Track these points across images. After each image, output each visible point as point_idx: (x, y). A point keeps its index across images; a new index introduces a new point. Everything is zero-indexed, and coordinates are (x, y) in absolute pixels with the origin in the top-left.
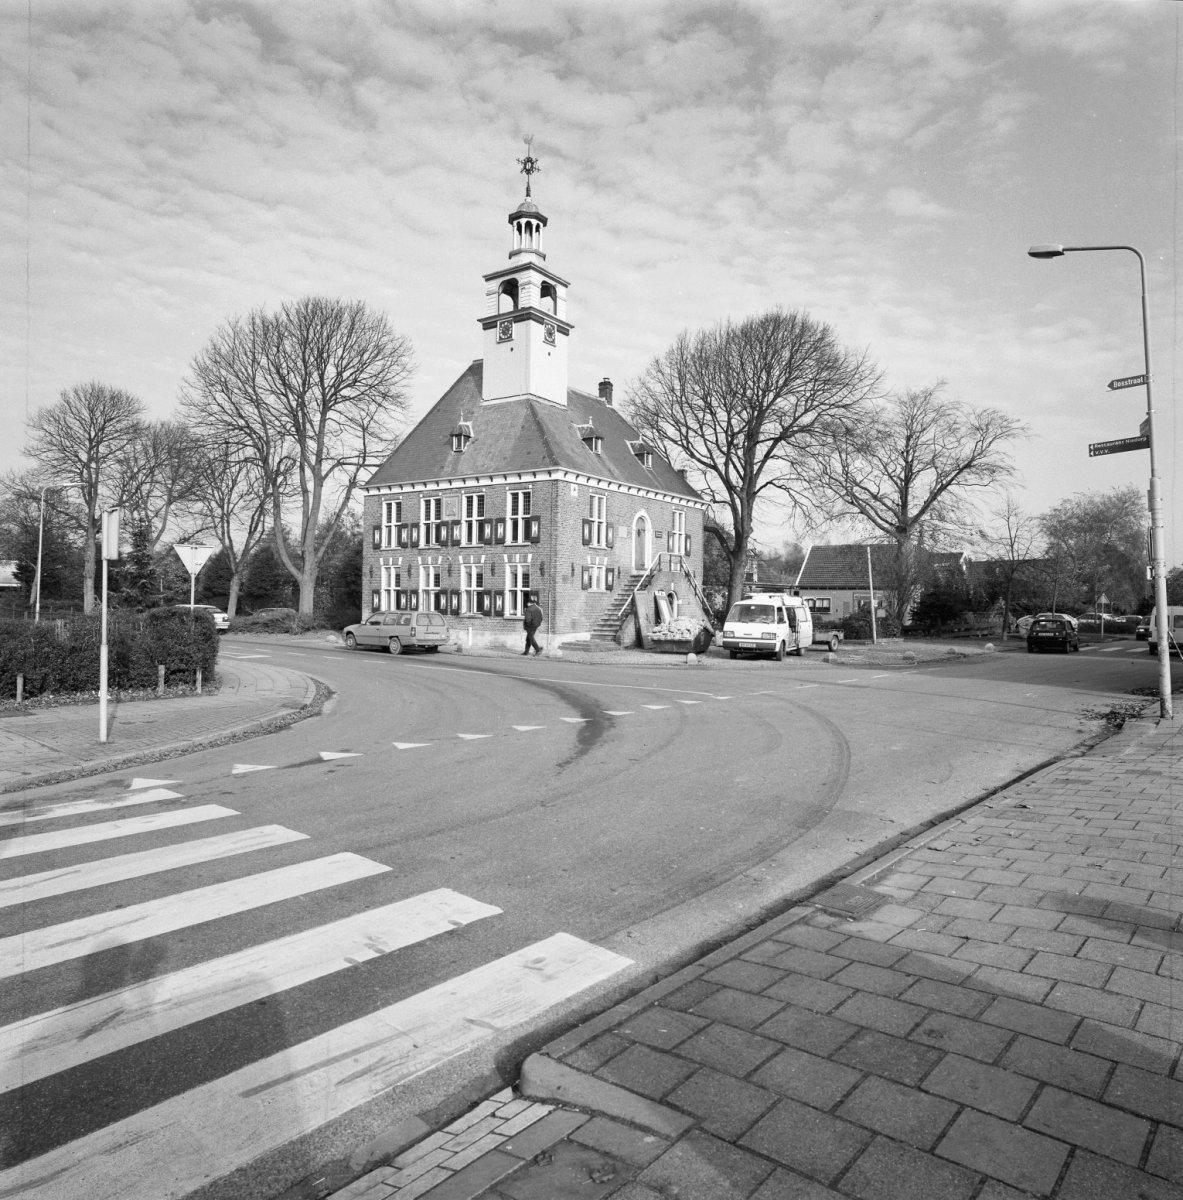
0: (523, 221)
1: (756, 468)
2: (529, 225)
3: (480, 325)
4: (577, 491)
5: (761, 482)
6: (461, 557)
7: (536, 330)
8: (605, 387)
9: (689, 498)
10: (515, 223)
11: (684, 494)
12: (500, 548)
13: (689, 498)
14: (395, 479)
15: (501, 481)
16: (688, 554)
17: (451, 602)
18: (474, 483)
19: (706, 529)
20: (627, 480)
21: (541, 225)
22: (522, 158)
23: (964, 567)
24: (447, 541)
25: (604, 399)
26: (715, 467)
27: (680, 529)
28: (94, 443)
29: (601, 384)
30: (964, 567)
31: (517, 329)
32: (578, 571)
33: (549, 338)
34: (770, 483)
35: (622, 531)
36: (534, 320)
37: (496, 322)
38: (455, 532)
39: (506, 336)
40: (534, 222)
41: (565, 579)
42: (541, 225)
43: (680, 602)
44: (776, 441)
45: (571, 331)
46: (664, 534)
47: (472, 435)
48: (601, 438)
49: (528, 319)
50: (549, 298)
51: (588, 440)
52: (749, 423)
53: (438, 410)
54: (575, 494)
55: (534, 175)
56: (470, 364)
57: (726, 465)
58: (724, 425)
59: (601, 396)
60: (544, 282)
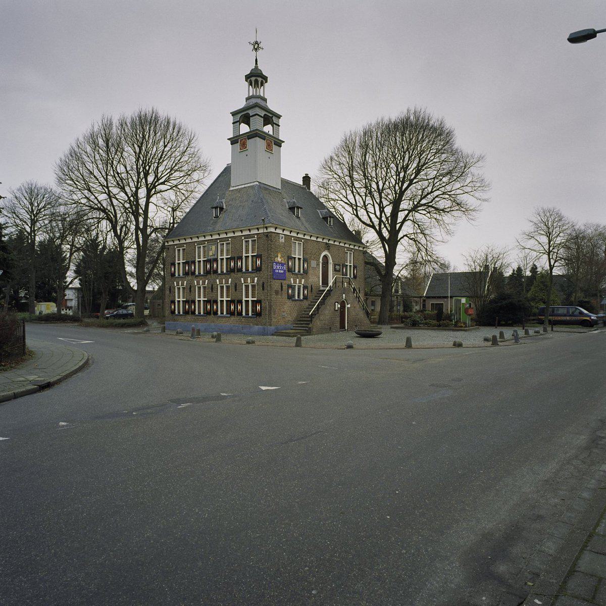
0: (253, 79)
1: (398, 226)
2: (256, 81)
3: (229, 142)
4: (283, 238)
5: (400, 235)
6: (218, 280)
7: (260, 143)
8: (307, 179)
9: (351, 243)
10: (248, 80)
11: (352, 241)
12: (240, 274)
13: (351, 243)
14: (176, 236)
15: (239, 234)
16: (355, 277)
17: (191, 307)
18: (224, 236)
19: (366, 263)
20: (339, 238)
21: (264, 81)
22: (252, 42)
23: (100, 247)
24: (188, 273)
25: (304, 186)
26: (373, 227)
27: (350, 263)
28: (34, 222)
29: (304, 178)
30: (100, 247)
31: (250, 143)
32: (285, 287)
33: (269, 147)
34: (406, 236)
35: (313, 263)
36: (258, 137)
37: (238, 139)
38: (233, 264)
39: (244, 146)
40: (260, 79)
41: (277, 293)
42: (264, 81)
43: (349, 306)
44: (410, 211)
45: (283, 144)
46: (340, 267)
47: (224, 207)
48: (301, 208)
49: (255, 137)
50: (270, 125)
51: (292, 209)
52: (353, 178)
53: (207, 194)
54: (283, 240)
55: (260, 51)
56: (225, 166)
57: (380, 225)
58: (378, 201)
59: (304, 184)
60: (265, 115)
